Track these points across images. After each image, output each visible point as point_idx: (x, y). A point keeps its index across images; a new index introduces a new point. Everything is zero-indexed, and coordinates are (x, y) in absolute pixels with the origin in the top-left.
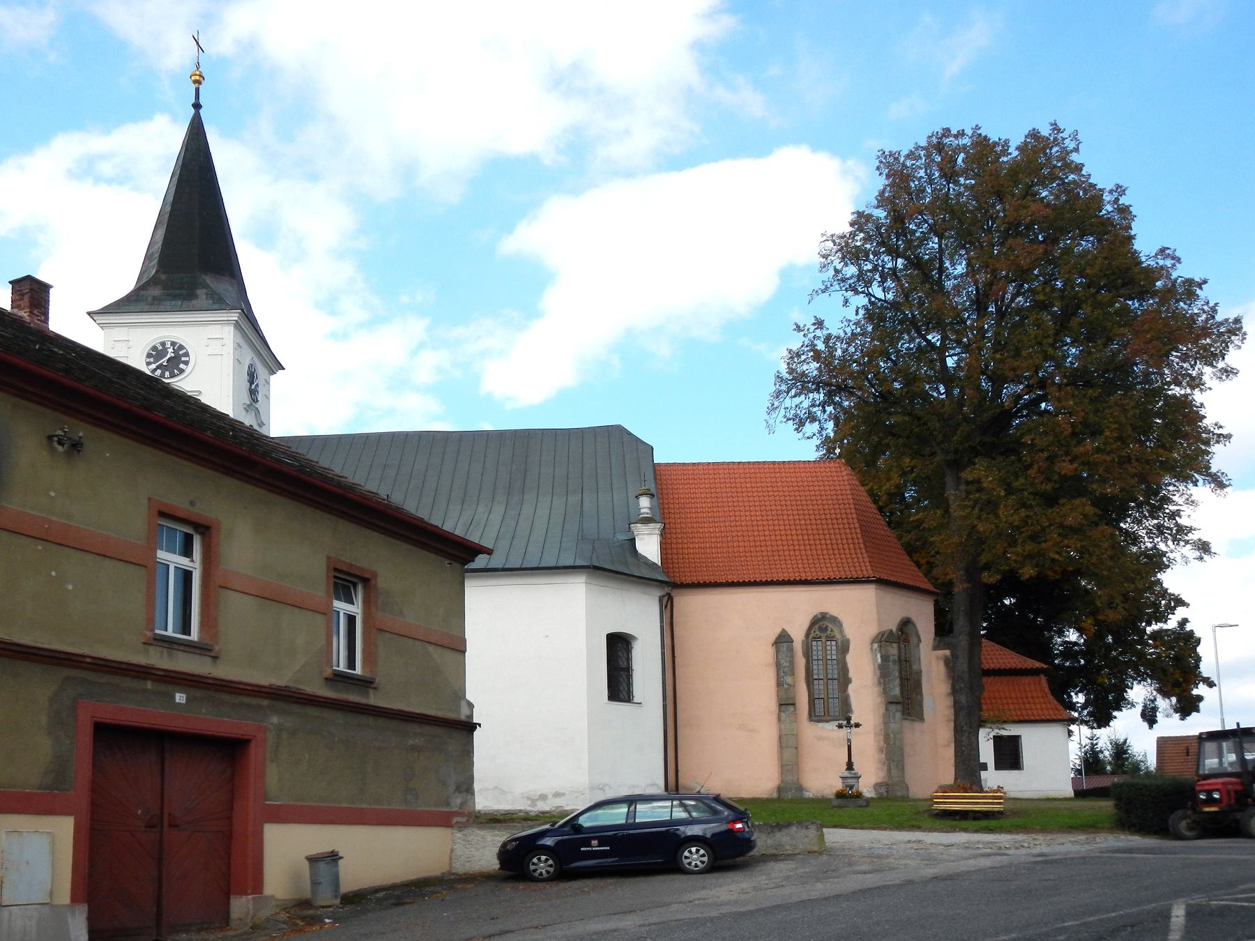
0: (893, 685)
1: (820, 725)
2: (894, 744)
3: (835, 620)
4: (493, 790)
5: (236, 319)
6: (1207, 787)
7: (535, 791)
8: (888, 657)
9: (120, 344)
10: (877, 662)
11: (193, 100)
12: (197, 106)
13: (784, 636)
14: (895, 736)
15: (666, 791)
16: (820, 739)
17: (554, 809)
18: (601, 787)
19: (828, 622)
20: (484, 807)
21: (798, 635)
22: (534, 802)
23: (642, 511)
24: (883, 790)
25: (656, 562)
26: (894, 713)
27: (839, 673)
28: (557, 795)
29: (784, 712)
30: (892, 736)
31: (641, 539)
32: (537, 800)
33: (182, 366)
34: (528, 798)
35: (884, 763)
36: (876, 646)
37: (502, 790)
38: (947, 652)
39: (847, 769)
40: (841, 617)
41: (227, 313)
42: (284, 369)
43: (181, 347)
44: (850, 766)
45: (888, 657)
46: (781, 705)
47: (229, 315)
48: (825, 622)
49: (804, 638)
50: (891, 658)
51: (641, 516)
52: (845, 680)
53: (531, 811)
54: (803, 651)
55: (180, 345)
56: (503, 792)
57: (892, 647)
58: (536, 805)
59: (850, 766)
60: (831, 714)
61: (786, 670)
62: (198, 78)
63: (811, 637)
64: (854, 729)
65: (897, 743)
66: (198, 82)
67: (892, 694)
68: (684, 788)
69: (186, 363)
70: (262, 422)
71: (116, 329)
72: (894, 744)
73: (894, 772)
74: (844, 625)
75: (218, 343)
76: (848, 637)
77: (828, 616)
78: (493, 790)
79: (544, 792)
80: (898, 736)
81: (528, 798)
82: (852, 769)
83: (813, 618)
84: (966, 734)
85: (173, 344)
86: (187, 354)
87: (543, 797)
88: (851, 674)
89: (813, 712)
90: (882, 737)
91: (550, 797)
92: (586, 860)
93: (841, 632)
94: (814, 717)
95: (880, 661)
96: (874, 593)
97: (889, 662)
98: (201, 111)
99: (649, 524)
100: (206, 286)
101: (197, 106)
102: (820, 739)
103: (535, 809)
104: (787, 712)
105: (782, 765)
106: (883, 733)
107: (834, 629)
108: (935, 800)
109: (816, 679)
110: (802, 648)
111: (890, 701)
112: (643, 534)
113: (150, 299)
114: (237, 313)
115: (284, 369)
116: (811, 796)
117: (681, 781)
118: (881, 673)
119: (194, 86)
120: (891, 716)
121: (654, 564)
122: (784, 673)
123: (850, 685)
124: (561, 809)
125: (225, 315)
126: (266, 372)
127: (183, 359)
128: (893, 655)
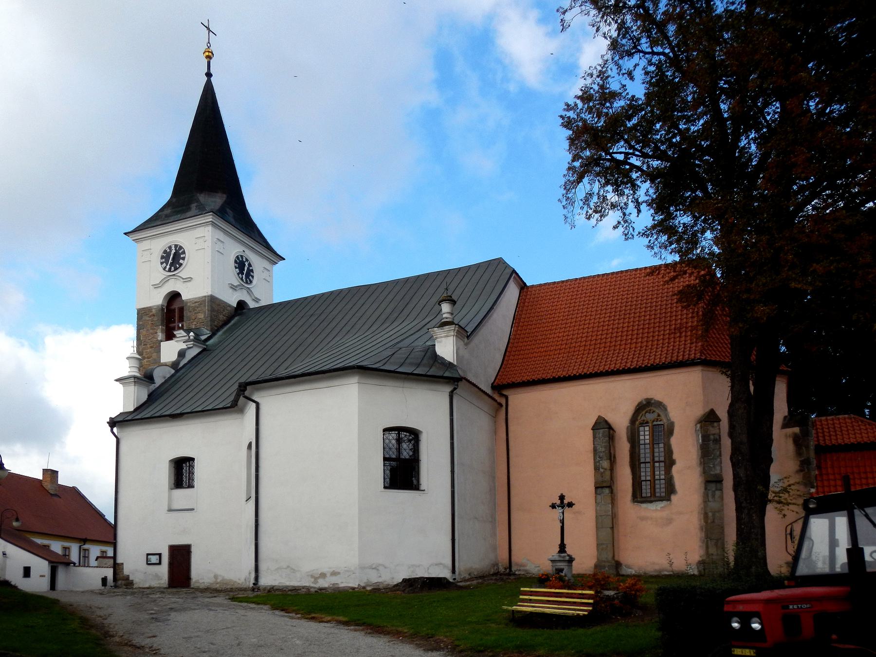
0: (714, 464)
1: (644, 505)
2: (713, 522)
3: (660, 405)
4: (286, 569)
5: (211, 220)
6: (741, 608)
7: (317, 570)
8: (709, 436)
9: (146, 253)
10: (699, 442)
11: (206, 71)
12: (209, 75)
13: (600, 423)
14: (714, 515)
15: (103, 586)
16: (643, 519)
17: (331, 586)
18: (374, 567)
19: (655, 407)
20: (280, 583)
21: (621, 421)
22: (316, 579)
23: (444, 316)
24: (701, 568)
25: (452, 361)
26: (714, 492)
27: (665, 455)
28: (334, 574)
29: (599, 494)
30: (710, 514)
31: (440, 342)
32: (319, 578)
33: (181, 261)
34: (312, 576)
35: (704, 541)
36: (699, 426)
37: (292, 569)
38: (797, 430)
39: (560, 552)
40: (666, 401)
41: (204, 217)
42: (284, 259)
43: (181, 248)
44: (562, 548)
45: (709, 436)
46: (596, 488)
47: (206, 218)
48: (652, 408)
49: (629, 425)
50: (712, 437)
51: (443, 321)
52: (670, 462)
53: (312, 587)
54: (628, 437)
55: (180, 246)
56: (294, 571)
57: (713, 427)
58: (317, 582)
59: (562, 548)
60: (658, 495)
61: (601, 455)
62: (210, 54)
63: (637, 423)
64: (567, 509)
65: (716, 521)
66: (209, 58)
67: (712, 473)
68: (517, 564)
69: (184, 259)
70: (256, 298)
71: (144, 242)
72: (713, 522)
73: (712, 550)
74: (669, 409)
75: (201, 240)
76: (672, 420)
77: (653, 401)
78: (286, 569)
79: (324, 570)
80: (717, 514)
81: (312, 576)
82: (565, 552)
83: (638, 405)
84: (746, 511)
85: (176, 246)
86: (184, 253)
87: (323, 575)
88: (675, 456)
89: (638, 493)
90: (702, 516)
91: (328, 575)
92: (809, 586)
93: (667, 415)
94: (638, 497)
95: (701, 441)
96: (700, 375)
97: (709, 441)
98: (212, 79)
99: (444, 327)
100: (198, 201)
101: (209, 75)
102: (643, 519)
103: (317, 586)
104: (602, 495)
105: (597, 545)
106: (703, 512)
107: (661, 413)
108: (521, 597)
109: (662, 462)
110: (627, 433)
111: (709, 479)
112: (441, 337)
113: (164, 216)
114: (210, 215)
115: (284, 259)
116: (634, 572)
117: (514, 558)
118: (702, 453)
119: (206, 61)
120: (710, 495)
121: (450, 363)
122: (599, 457)
123: (674, 466)
124: (336, 586)
125: (203, 218)
126: (266, 264)
127: (182, 256)
128: (714, 434)
